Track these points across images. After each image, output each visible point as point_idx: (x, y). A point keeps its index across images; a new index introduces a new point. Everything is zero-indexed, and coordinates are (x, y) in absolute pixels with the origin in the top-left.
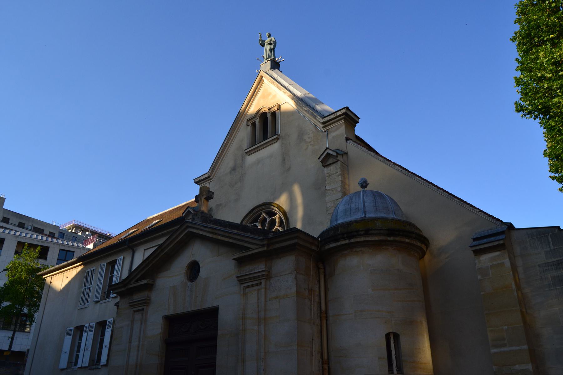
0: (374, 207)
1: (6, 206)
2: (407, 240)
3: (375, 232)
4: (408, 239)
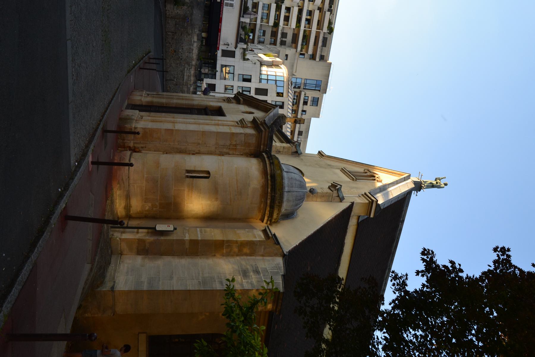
0: (292, 178)
1: (313, 119)
2: (269, 190)
3: (272, 167)
4: (270, 191)
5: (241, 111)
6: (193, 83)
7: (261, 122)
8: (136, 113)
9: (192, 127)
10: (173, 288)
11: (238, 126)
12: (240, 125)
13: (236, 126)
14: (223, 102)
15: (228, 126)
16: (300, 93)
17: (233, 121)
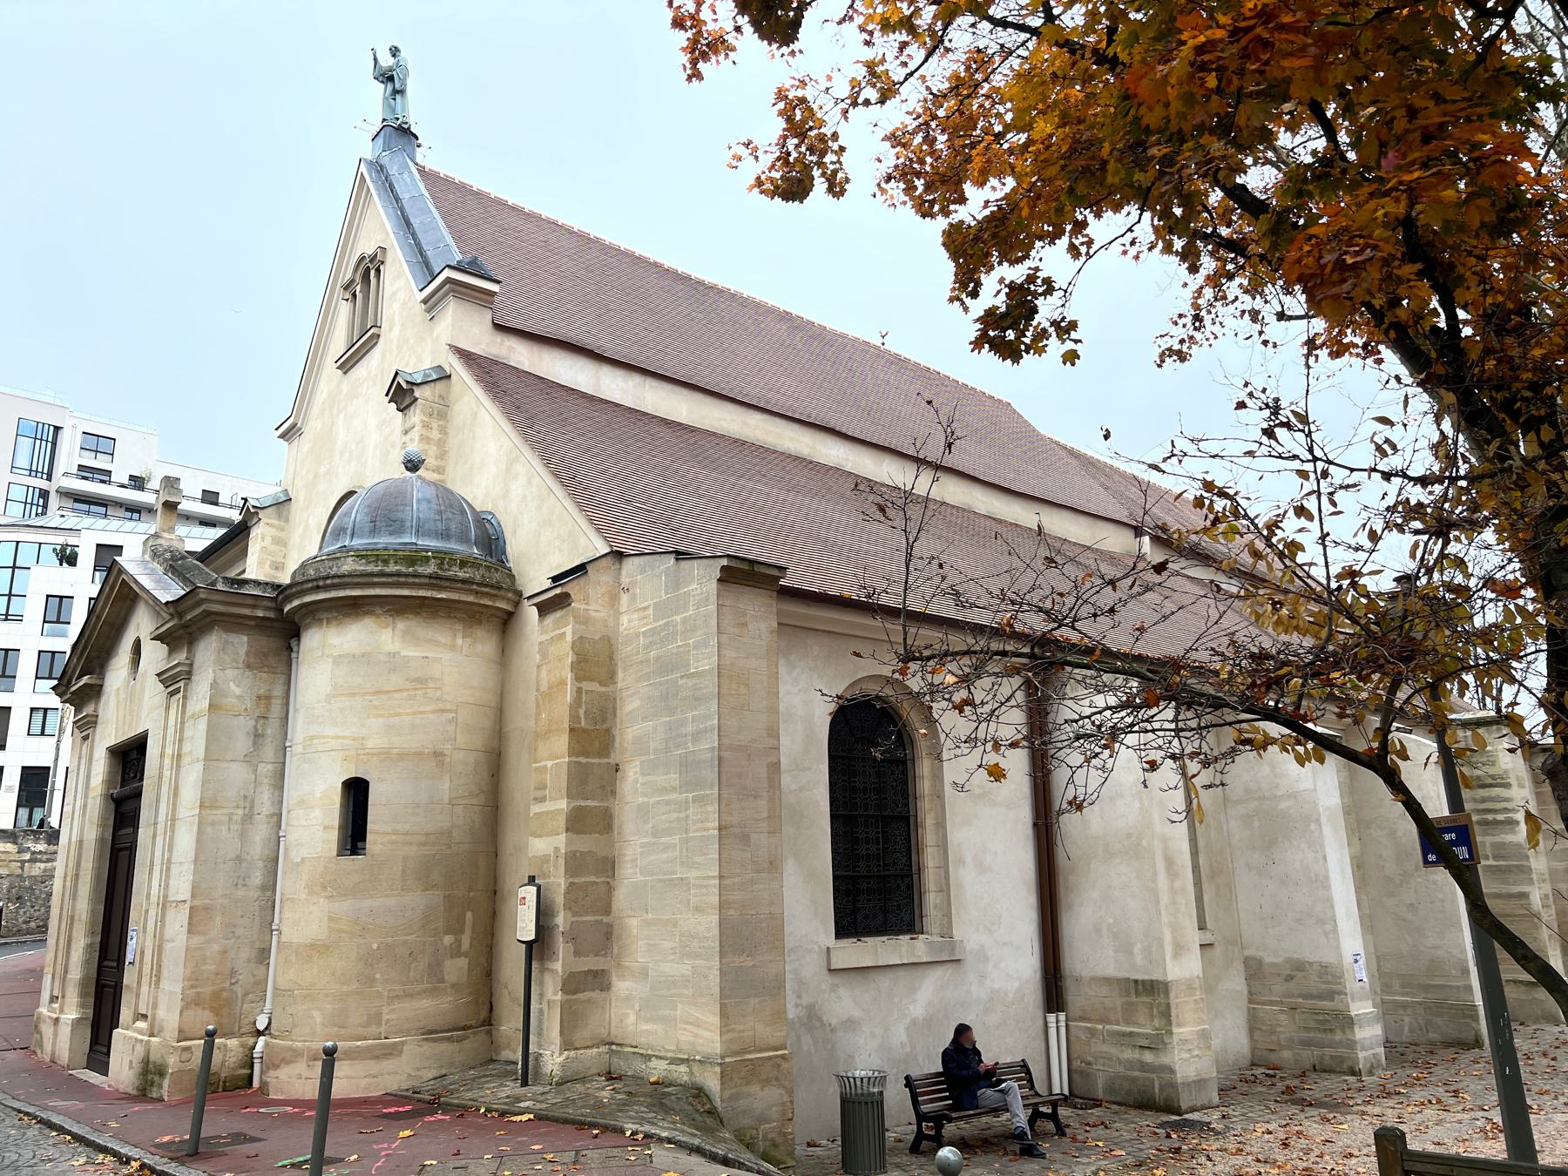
5: (129, 682)
6: (15, 843)
7: (171, 615)
8: (127, 1042)
9: (185, 841)
10: (714, 877)
11: (185, 691)
12: (181, 684)
13: (185, 697)
14: (93, 741)
15: (183, 723)
16: (65, 494)
17: (168, 708)
